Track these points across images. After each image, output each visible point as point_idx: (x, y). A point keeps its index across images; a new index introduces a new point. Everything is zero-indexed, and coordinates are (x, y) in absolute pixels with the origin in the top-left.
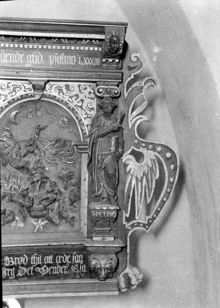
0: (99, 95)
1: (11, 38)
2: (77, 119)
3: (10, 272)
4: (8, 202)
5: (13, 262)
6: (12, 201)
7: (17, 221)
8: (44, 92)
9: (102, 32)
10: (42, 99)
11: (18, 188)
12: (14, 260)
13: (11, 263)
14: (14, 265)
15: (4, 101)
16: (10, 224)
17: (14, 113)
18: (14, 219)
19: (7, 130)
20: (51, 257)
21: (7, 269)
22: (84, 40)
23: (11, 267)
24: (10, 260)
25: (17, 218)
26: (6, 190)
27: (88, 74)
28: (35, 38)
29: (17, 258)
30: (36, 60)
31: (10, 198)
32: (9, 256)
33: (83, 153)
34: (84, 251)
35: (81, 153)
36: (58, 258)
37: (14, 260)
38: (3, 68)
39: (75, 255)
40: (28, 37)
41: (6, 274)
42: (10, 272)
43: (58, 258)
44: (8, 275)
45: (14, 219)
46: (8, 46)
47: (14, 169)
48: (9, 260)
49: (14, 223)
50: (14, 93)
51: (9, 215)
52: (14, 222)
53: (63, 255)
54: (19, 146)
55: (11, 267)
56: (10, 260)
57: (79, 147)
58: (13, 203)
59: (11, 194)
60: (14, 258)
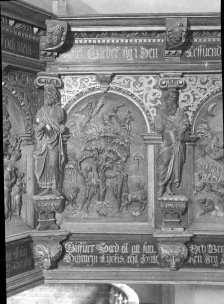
0: (164, 87)
1: (93, 34)
2: (144, 111)
3: (213, 259)
4: (208, 192)
5: (216, 250)
6: (212, 191)
7: (217, 210)
8: (110, 84)
9: (164, 25)
10: (109, 91)
11: (216, 178)
12: (217, 248)
13: (214, 251)
14: (217, 253)
15: (204, 94)
16: (210, 213)
17: (212, 105)
18: (214, 209)
19: (205, 122)
20: (138, 247)
21: (210, 256)
22: (103, 34)
23: (214, 255)
24: (213, 247)
25: (216, 207)
26: (205, 179)
27: (130, 68)
28: (85, 34)
29: (220, 246)
30: (201, 51)
31: (209, 188)
32: (212, 244)
33: (150, 144)
34: (154, 242)
35: (147, 144)
36: (117, 250)
37: (217, 248)
38: (72, 65)
39: (146, 245)
40: (109, 32)
41: (209, 261)
42: (213, 259)
43: (117, 250)
44: (212, 262)
45: (214, 209)
46: (82, 42)
47: (213, 161)
48: (212, 248)
49: (213, 213)
50: (213, 86)
51: (209, 205)
52: (214, 211)
53: (115, 245)
54: (217, 138)
55: (214, 255)
56: (213, 247)
57: (145, 137)
58: (213, 193)
59: (210, 184)
60: (216, 246)
